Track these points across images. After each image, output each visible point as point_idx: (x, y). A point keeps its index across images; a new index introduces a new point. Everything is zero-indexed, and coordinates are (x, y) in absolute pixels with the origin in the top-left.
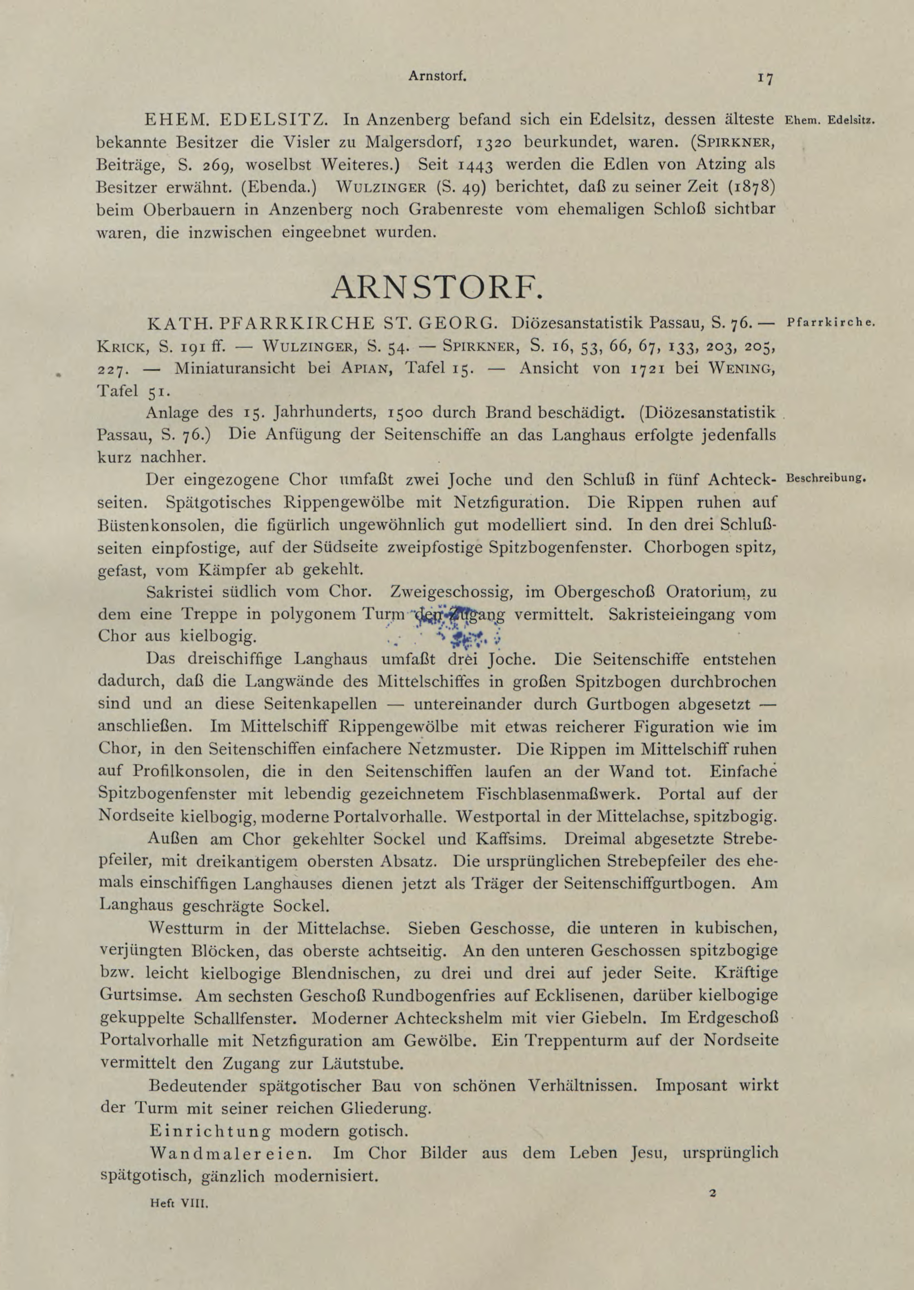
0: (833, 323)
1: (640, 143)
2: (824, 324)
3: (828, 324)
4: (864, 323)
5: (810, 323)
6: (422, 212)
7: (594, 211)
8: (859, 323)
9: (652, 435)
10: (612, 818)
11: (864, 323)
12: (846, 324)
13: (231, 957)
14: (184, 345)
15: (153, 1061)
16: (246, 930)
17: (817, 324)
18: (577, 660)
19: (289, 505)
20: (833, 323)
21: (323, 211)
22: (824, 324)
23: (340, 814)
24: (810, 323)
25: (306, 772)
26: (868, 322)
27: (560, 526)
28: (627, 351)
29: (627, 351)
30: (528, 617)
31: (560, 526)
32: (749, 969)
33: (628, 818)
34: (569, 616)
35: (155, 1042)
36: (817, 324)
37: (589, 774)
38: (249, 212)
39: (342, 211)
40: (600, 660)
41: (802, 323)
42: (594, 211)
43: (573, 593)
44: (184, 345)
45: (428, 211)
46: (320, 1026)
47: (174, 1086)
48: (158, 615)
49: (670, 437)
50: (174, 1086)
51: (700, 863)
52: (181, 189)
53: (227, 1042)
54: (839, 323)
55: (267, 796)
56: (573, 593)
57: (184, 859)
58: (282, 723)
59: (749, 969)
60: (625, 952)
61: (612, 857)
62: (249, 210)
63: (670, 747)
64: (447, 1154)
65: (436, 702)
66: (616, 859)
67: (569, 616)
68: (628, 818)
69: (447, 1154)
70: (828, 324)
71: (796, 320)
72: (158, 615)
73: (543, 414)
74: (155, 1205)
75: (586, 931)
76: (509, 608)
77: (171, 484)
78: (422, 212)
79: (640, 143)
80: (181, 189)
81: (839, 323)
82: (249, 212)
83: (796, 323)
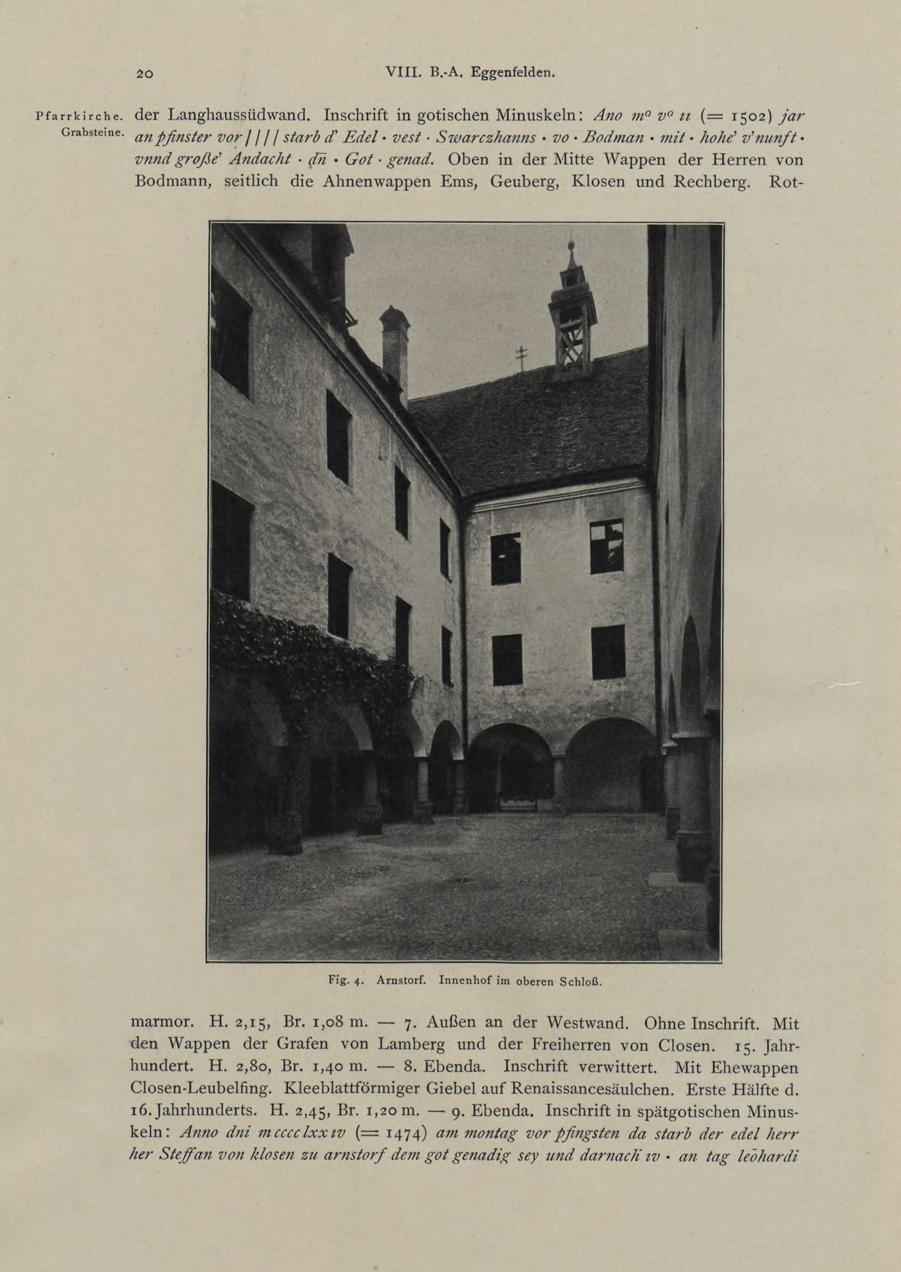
0: (81, 117)
1: (385, 183)
3: (76, 118)
4: (112, 117)
5: (59, 117)
6: (290, 1046)
7: (140, 1024)
10: (569, 161)
12: (94, 118)
17: (65, 118)
20: (81, 117)
21: (718, 183)
24: (59, 117)
25: (507, 161)
26: (116, 116)
33: (585, 160)
36: (65, 118)
37: (731, 162)
38: (503, 161)
39: (737, 183)
41: (50, 117)
42: (140, 1024)
43: (466, 161)
45: (295, 1045)
47: (643, 162)
50: (643, 162)
51: (540, 162)
54: (87, 117)
56: (466, 161)
62: (503, 160)
68: (585, 160)
70: (76, 118)
71: (45, 114)
74: (719, 162)
78: (290, 1046)
79: (385, 183)
81: (87, 117)
82: (503, 161)
83: (45, 116)
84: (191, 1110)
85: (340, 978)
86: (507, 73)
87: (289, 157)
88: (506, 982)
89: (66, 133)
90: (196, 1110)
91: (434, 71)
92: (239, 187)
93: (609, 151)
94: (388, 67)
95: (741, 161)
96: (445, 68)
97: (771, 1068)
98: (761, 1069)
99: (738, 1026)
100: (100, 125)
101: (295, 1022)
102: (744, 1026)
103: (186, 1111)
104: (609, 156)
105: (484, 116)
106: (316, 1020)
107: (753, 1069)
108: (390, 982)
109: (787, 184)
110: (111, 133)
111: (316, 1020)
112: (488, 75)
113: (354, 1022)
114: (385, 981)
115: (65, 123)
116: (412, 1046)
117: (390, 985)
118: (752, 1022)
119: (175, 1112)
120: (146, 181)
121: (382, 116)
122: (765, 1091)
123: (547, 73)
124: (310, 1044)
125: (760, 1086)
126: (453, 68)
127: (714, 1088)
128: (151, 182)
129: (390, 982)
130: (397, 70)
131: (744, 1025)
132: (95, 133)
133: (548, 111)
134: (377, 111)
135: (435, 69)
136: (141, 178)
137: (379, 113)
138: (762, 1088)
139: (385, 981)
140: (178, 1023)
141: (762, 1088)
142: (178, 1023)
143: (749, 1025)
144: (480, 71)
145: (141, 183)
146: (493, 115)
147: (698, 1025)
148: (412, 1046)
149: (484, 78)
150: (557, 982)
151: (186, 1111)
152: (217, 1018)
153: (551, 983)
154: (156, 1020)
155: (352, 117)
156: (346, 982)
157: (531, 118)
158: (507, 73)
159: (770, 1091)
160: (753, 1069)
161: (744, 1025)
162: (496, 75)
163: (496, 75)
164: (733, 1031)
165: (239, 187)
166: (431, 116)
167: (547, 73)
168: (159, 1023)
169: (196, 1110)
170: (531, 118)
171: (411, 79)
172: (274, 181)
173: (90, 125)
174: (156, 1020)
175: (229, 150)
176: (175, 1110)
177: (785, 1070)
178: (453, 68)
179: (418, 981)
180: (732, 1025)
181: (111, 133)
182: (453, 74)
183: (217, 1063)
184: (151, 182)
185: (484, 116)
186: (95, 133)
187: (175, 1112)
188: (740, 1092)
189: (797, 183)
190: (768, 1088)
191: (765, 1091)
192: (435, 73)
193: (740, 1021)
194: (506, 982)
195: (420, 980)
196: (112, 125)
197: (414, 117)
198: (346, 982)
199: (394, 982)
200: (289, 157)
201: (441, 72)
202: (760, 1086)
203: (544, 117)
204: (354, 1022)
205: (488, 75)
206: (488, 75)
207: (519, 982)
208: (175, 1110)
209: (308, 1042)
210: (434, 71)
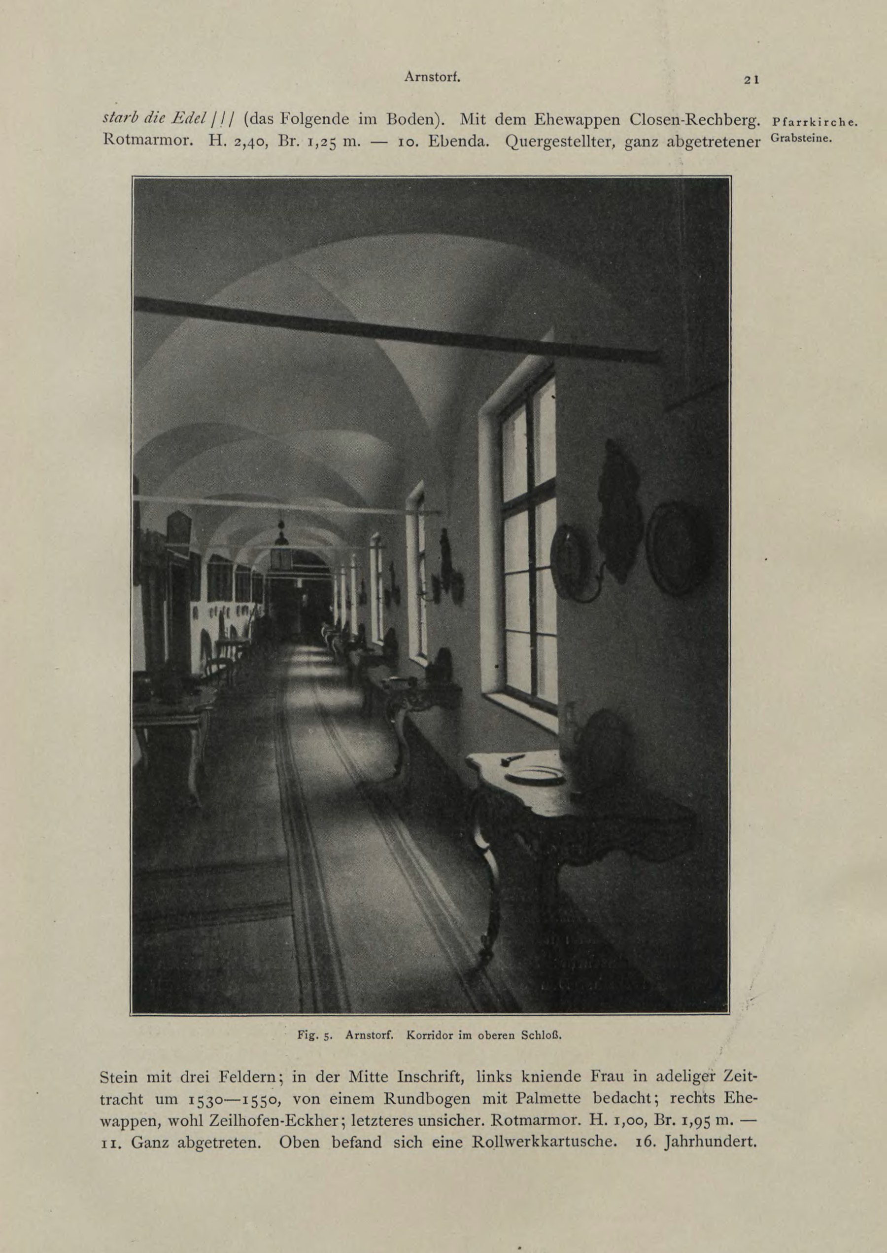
0: (817, 123)
2: (808, 124)
4: (847, 123)
5: (795, 123)
8: (842, 123)
11: (847, 123)
12: (829, 124)
14: (401, 140)
15: (569, 1096)
17: (802, 124)
18: (383, 1078)
19: (496, 1123)
20: (817, 123)
24: (795, 123)
32: (454, 1073)
34: (379, 1078)
36: (802, 124)
40: (404, 1077)
41: (787, 123)
44: (401, 140)
46: (357, 1084)
48: (347, 1100)
53: (156, 1077)
54: (823, 123)
55: (166, 1079)
57: (504, 1097)
59: (454, 1073)
60: (425, 1078)
61: (104, 1074)
63: (377, 1075)
64: (247, 1078)
66: (109, 1076)
67: (379, 1078)
69: (247, 1078)
72: (347, 1100)
73: (598, 1099)
75: (577, 1079)
85: (308, 1033)
88: (468, 1036)
92: (611, 126)
97: (130, 1122)
98: (120, 1122)
99: (443, 1079)
100: (808, 131)
101: (665, 1120)
102: (449, 1079)
106: (685, 1119)
107: (111, 1122)
108: (359, 1037)
110: (819, 139)
111: (685, 1119)
113: (151, 1078)
114: (354, 1036)
117: (359, 1040)
118: (457, 1075)
120: (397, 119)
124: (261, 1121)
128: (402, 121)
129: (359, 1037)
131: (449, 1077)
136: (392, 116)
137: (451, 1075)
139: (354, 1036)
140: (566, 1121)
142: (566, 1121)
143: (454, 1078)
145: (393, 121)
147: (403, 1078)
150: (518, 1036)
152: (596, 1116)
153: (512, 1037)
154: (543, 1119)
156: (315, 1037)
160: (111, 1122)
161: (449, 1077)
164: (438, 1084)
168: (546, 1121)
173: (800, 131)
174: (543, 1119)
177: (144, 1123)
179: (386, 1036)
180: (438, 1077)
181: (819, 139)
184: (402, 121)
193: (445, 1073)
194: (468, 1036)
195: (387, 1035)
198: (315, 1037)
199: (363, 1036)
204: (151, 1078)
207: (480, 1037)
209: (259, 1119)
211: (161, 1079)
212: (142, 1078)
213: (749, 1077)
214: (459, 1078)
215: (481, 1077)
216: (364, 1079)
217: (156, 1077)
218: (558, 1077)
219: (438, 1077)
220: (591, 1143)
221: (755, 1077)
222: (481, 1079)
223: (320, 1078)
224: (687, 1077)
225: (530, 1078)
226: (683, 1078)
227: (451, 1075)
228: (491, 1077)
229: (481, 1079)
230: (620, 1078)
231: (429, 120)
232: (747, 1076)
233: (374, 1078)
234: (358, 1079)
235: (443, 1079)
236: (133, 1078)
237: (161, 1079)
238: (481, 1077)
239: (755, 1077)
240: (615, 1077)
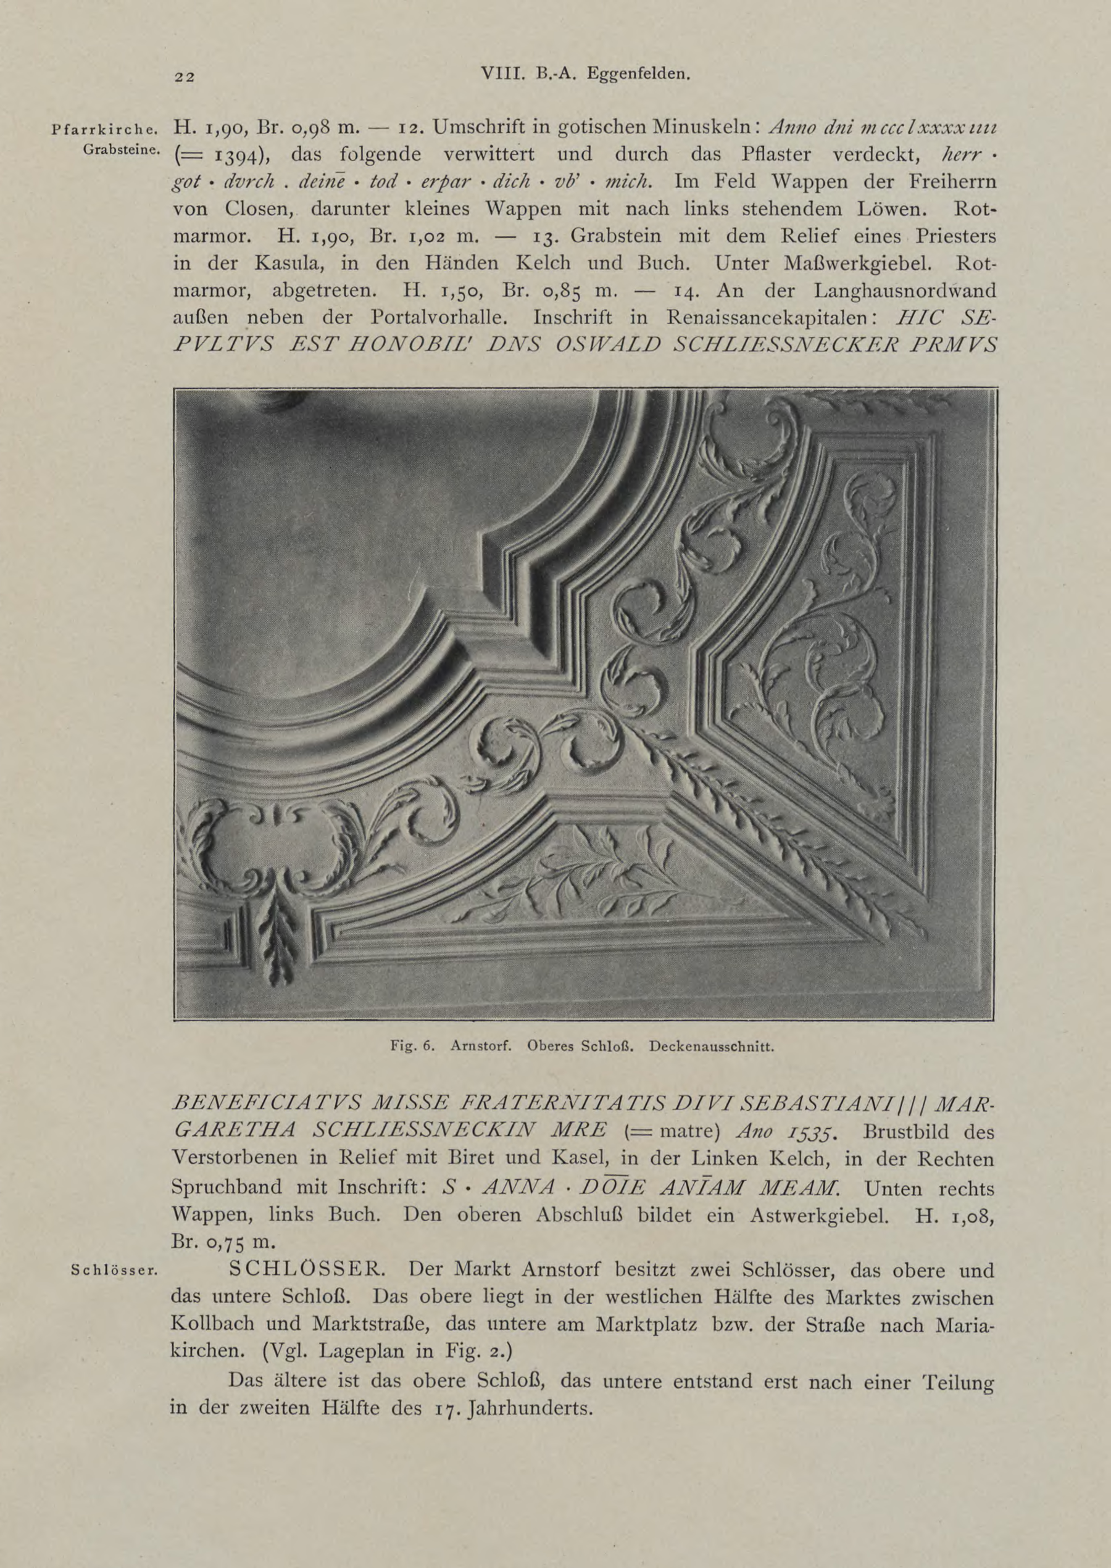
0: (107, 131)
2: (96, 131)
4: (144, 130)
5: (80, 131)
9: (802, 128)
13: (902, 162)
16: (656, 236)
17: (88, 131)
20: (107, 131)
22: (96, 131)
23: (378, 313)
24: (80, 131)
27: (527, 156)
28: (243, 133)
29: (243, 133)
30: (460, 157)
31: (527, 156)
33: (508, 155)
35: (437, 320)
36: (88, 131)
37: (881, 185)
40: (622, 1270)
41: (70, 131)
49: (365, 157)
51: (887, 184)
52: (473, 156)
54: (115, 131)
58: (738, 178)
64: (667, 1217)
65: (367, 206)
66: (182, 1185)
68: (508, 155)
69: (667, 1217)
71: (63, 127)
75: (417, 157)
76: (333, 1197)
77: (889, 187)
80: (473, 156)
81: (115, 131)
83: (63, 130)
84: (512, 1408)
86: (631, 74)
87: (198, 179)
89: (88, 150)
90: (518, 1409)
91: (542, 72)
93: (778, 172)
94: (484, 68)
95: (976, 183)
96: (554, 69)
99: (396, 1189)
100: (130, 141)
103: (505, 1410)
104: (779, 177)
105: (641, 128)
109: (976, 211)
110: (145, 151)
112: (608, 77)
115: (87, 138)
116: (236, 1190)
119: (492, 1411)
121: (518, 128)
122: (755, 1298)
123: (681, 75)
125: (748, 1293)
126: (565, 68)
127: (217, 1155)
130: (495, 70)
131: (599, 318)
132: (125, 150)
133: (716, 122)
134: (511, 122)
135: (542, 70)
137: (514, 124)
138: (751, 1295)
141: (751, 1295)
144: (598, 73)
146: (651, 126)
148: (236, 1190)
149: (603, 80)
151: (505, 1410)
155: (481, 128)
157: (696, 130)
158: (631, 74)
159: (761, 1298)
161: (599, 318)
162: (618, 77)
163: (618, 77)
165: (381, 216)
166: (575, 128)
167: (681, 75)
169: (518, 1409)
170: (696, 130)
171: (513, 81)
172: (664, 209)
173: (120, 141)
175: (223, 172)
176: (492, 1409)
178: (565, 68)
181: (145, 151)
182: (564, 76)
183: (274, 1265)
185: (641, 128)
186: (125, 150)
187: (492, 1411)
188: (723, 1299)
189: (988, 210)
190: (758, 1295)
191: (755, 1298)
192: (543, 75)
196: (146, 141)
197: (554, 130)
200: (198, 179)
201: (550, 73)
202: (748, 1293)
203: (711, 130)
204: (584, 210)
205: (608, 77)
206: (608, 77)
208: (492, 1409)
210: (542, 72)
211: (424, 1160)
212: (737, 1269)
213: (989, 1272)
214: (914, 157)
215: (275, 1215)
216: (671, 128)
217: (308, 1188)
218: (796, 210)
219: (389, 1188)
220: (609, 128)
221: (994, 210)
222: (275, 1217)
223: (789, 1299)
224: (814, 237)
225: (360, 1325)
226: (733, 129)
227: (514, 124)
228: (287, 1215)
229: (275, 1217)
230: (940, 1272)
231: (745, 128)
232: (281, 1408)
233: (501, 155)
234: (324, 1327)
235: (396, 1189)
236: (642, 318)
237: (424, 1160)
238: (275, 1215)
239: (994, 210)
240: (882, 291)
